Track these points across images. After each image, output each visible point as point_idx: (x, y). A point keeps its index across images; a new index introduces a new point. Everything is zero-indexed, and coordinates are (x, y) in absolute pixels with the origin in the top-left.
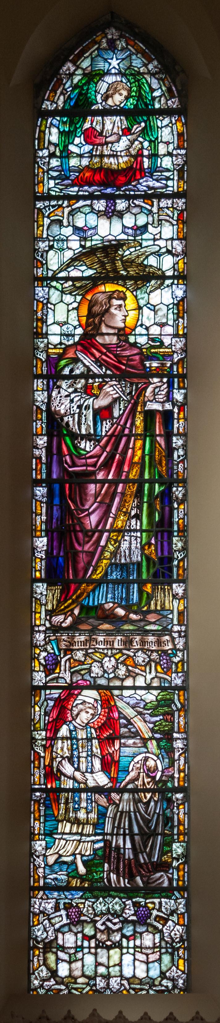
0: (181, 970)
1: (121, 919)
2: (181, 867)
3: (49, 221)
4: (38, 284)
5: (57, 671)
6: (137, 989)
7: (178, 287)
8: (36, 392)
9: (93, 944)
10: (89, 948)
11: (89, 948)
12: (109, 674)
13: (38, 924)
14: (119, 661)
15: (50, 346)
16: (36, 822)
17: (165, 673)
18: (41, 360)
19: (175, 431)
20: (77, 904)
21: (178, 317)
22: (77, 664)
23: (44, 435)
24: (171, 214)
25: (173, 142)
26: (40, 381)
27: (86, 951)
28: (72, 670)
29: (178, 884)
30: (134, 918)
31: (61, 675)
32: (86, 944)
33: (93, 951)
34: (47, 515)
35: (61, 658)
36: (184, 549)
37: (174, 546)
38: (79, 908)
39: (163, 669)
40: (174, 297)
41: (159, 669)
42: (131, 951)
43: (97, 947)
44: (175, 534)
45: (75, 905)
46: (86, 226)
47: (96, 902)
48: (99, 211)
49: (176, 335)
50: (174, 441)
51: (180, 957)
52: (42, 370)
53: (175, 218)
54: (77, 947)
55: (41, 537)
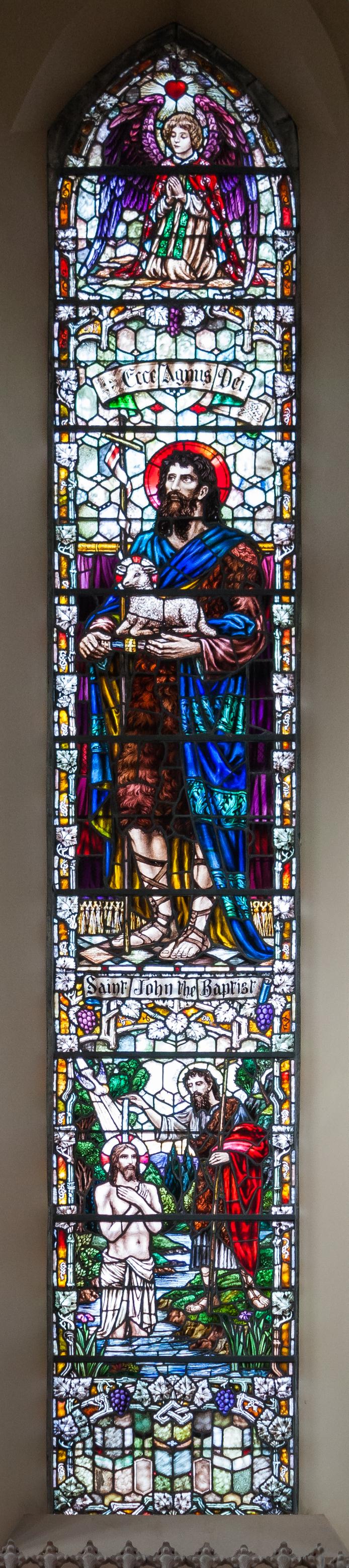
0: (284, 1483)
1: (193, 1407)
2: (284, 1327)
3: (76, 343)
4: (61, 438)
5: (97, 1030)
6: (218, 1509)
7: (282, 445)
8: (58, 607)
9: (148, 1444)
10: (143, 1448)
11: (143, 1448)
12: (176, 1035)
13: (66, 1415)
14: (191, 1019)
15: (80, 539)
16: (61, 1262)
17: (263, 1033)
18: (67, 557)
19: (277, 666)
20: (124, 1384)
21: (283, 492)
22: (290, 262)
23: (72, 674)
24: (271, 331)
25: (274, 212)
26: (64, 733)
27: (137, 1453)
28: (119, 1030)
29: (280, 1352)
30: (212, 1406)
31: (102, 1037)
32: (138, 1442)
33: (148, 1454)
34: (76, 794)
35: (102, 1015)
36: (294, 845)
37: (275, 841)
38: (126, 1390)
39: (259, 1028)
40: (276, 460)
41: (254, 1028)
42: (207, 1454)
43: (154, 1448)
44: (278, 822)
45: (120, 1385)
46: (136, 332)
47: (153, 1382)
48: (160, 327)
49: (277, 519)
50: (274, 682)
51: (282, 1463)
52: (69, 730)
53: (278, 337)
54: (123, 1448)
55: (68, 825)
